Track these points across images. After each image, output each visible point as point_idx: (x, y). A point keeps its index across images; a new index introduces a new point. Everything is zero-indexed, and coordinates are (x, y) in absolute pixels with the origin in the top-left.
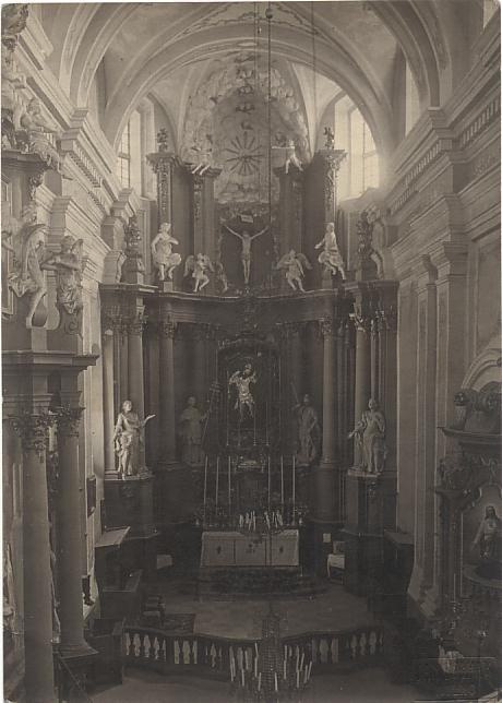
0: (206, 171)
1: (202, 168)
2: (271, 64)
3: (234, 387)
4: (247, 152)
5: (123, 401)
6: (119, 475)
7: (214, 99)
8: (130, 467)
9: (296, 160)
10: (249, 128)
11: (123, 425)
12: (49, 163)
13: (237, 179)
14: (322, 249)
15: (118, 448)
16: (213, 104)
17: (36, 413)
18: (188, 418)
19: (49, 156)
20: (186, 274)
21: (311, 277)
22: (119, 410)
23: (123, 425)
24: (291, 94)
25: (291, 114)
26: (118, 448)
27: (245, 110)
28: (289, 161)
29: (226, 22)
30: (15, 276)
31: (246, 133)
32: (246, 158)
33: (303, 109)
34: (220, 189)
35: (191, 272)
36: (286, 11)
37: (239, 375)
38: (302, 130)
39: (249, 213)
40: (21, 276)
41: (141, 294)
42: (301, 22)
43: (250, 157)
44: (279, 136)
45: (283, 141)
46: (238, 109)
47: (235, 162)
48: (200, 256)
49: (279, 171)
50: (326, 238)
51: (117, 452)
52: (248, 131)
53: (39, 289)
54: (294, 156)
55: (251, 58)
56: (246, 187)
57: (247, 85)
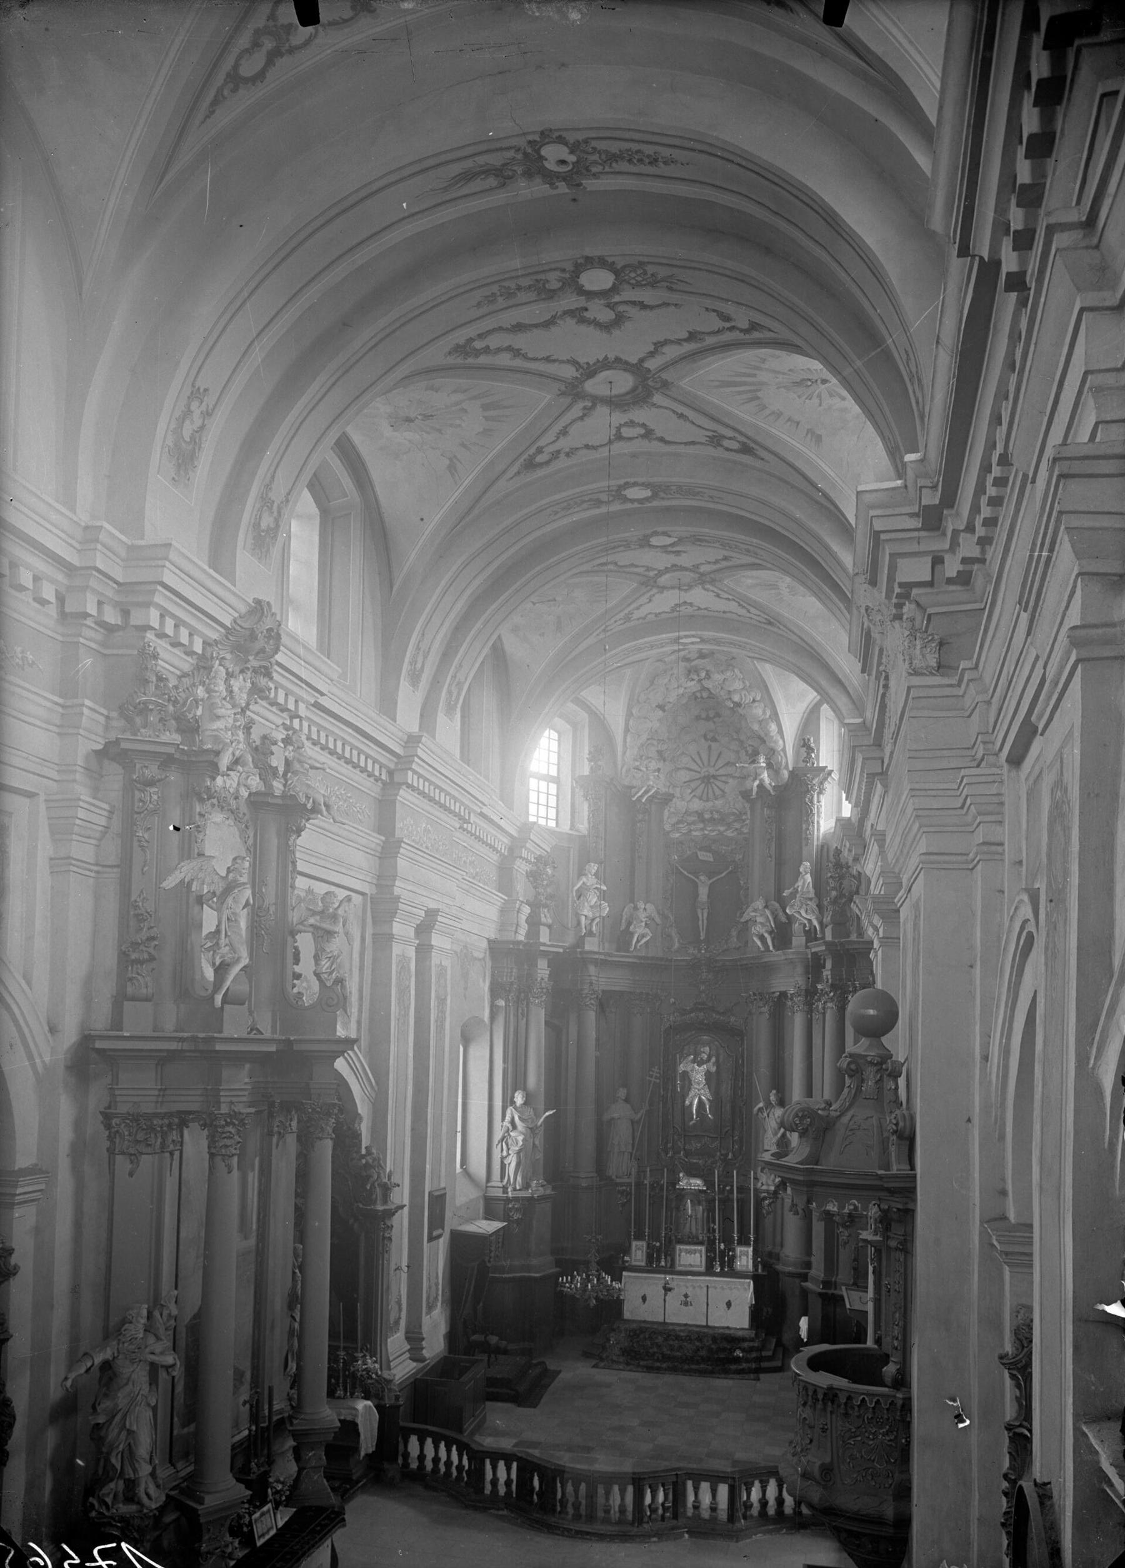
0: (652, 796)
1: (646, 792)
2: (730, 663)
3: (685, 1075)
4: (712, 771)
5: (515, 1090)
6: (505, 1189)
7: (661, 707)
8: (519, 1179)
9: (767, 781)
10: (714, 740)
11: (513, 1122)
12: (309, 806)
13: (697, 805)
14: (793, 895)
15: (505, 1153)
16: (660, 712)
17: (224, 1109)
18: (616, 1115)
19: (308, 798)
20: (623, 927)
21: (782, 934)
22: (508, 1101)
23: (513, 1122)
24: (758, 698)
25: (760, 722)
26: (505, 1153)
27: (708, 719)
28: (757, 783)
29: (656, 615)
30: (209, 944)
31: (710, 747)
32: (707, 780)
33: (775, 717)
34: (674, 820)
35: (629, 924)
36: (728, 599)
37: (694, 1061)
38: (776, 742)
39: (707, 849)
40: (217, 944)
41: (545, 954)
42: (748, 611)
43: (714, 777)
44: (750, 750)
45: (753, 757)
46: (698, 718)
47: (693, 785)
48: (641, 905)
49: (746, 795)
50: (800, 883)
51: (503, 1159)
52: (714, 745)
53: (238, 960)
54: (765, 775)
55: (702, 656)
56: (707, 816)
57: (704, 689)
